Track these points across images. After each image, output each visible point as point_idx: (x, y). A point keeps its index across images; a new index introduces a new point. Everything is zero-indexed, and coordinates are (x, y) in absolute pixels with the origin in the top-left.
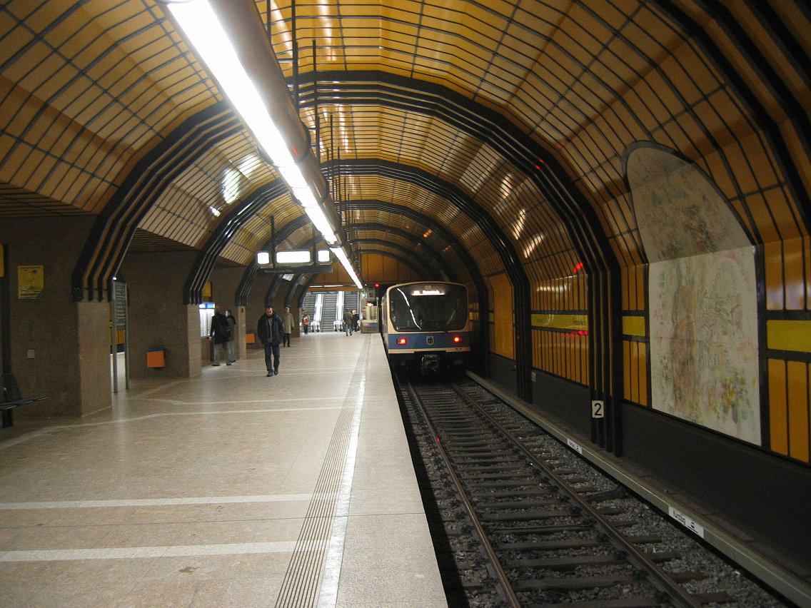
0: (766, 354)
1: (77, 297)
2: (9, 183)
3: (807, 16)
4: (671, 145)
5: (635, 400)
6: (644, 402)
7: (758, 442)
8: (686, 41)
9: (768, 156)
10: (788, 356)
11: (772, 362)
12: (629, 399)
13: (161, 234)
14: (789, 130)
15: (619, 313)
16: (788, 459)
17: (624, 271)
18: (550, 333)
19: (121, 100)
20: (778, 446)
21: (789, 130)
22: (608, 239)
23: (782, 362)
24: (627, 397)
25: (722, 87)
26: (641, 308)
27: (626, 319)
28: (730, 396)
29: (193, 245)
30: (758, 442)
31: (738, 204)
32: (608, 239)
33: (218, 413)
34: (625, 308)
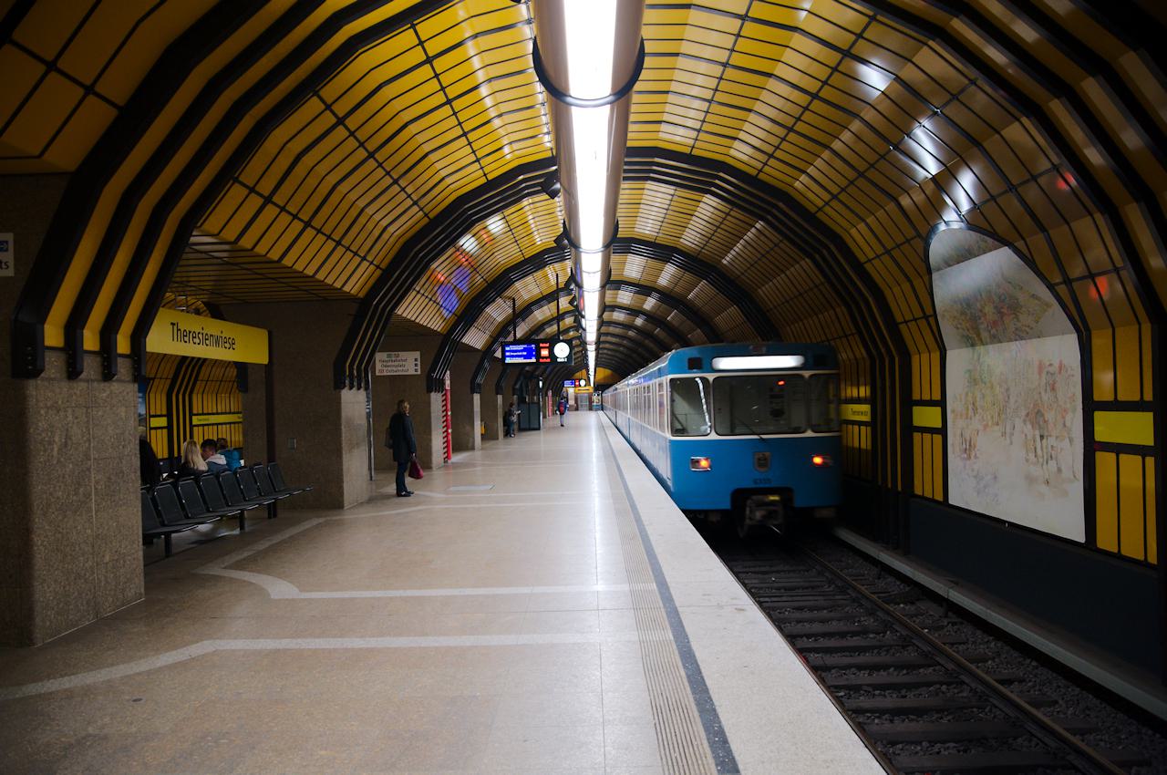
0: (1092, 447)
1: (339, 385)
2: (340, 289)
3: (1163, 85)
4: (989, 229)
5: (928, 494)
6: (939, 497)
7: (1082, 540)
8: (926, 44)
9: (1100, 234)
10: (1119, 449)
11: (1100, 456)
12: (920, 493)
13: (425, 324)
14: (1136, 217)
15: (909, 403)
16: (1118, 556)
17: (915, 360)
18: (857, 427)
19: (419, 203)
20: (1106, 541)
21: (1136, 217)
22: (316, 94)
23: (1113, 456)
24: (918, 491)
25: (872, 18)
26: (937, 397)
27: (916, 409)
28: (381, 371)
29: (439, 330)
30: (1082, 540)
31: (1062, 289)
32: (316, 94)
33: (473, 492)
34: (916, 396)
